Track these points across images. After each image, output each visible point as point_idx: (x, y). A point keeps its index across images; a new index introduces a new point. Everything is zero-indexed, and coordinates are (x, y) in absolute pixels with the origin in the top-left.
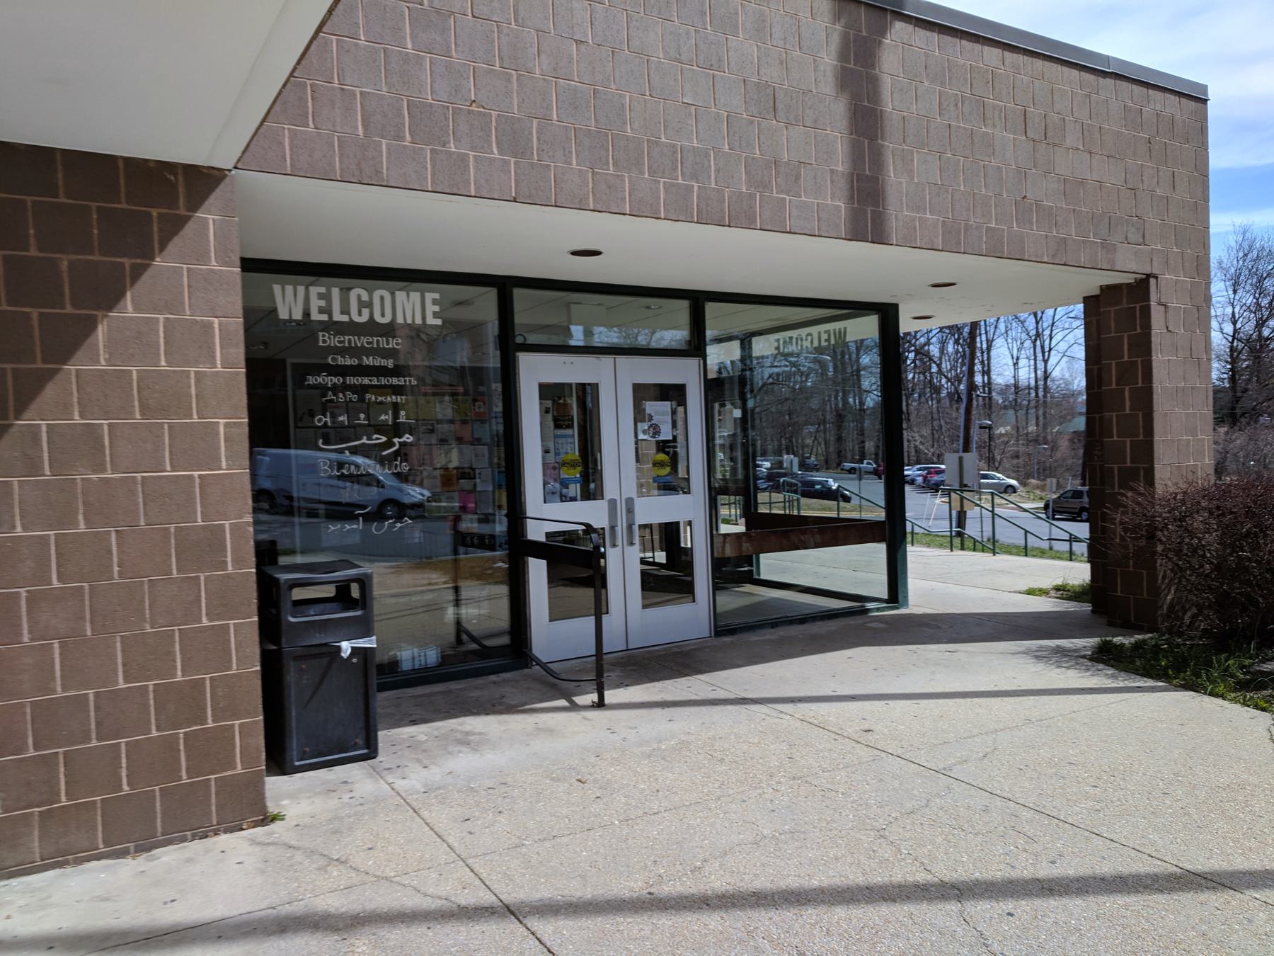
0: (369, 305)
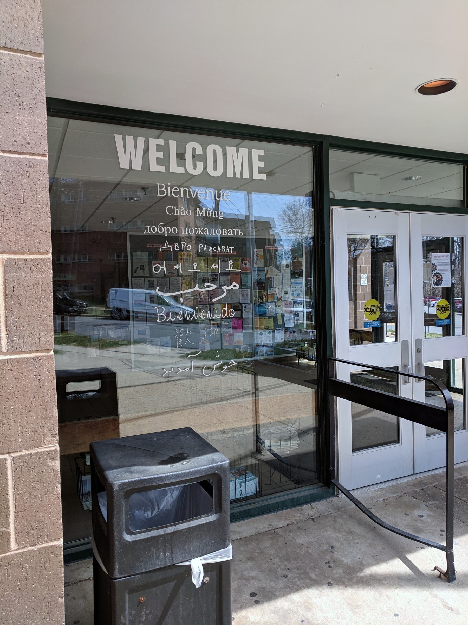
0: (203, 158)
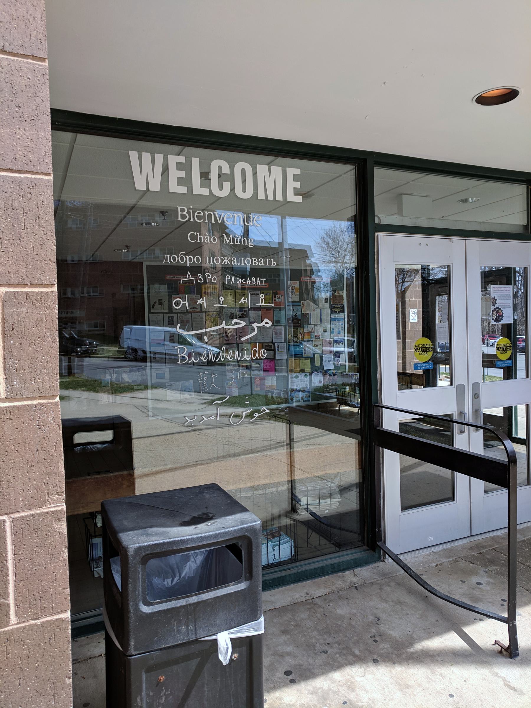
0: (230, 178)
